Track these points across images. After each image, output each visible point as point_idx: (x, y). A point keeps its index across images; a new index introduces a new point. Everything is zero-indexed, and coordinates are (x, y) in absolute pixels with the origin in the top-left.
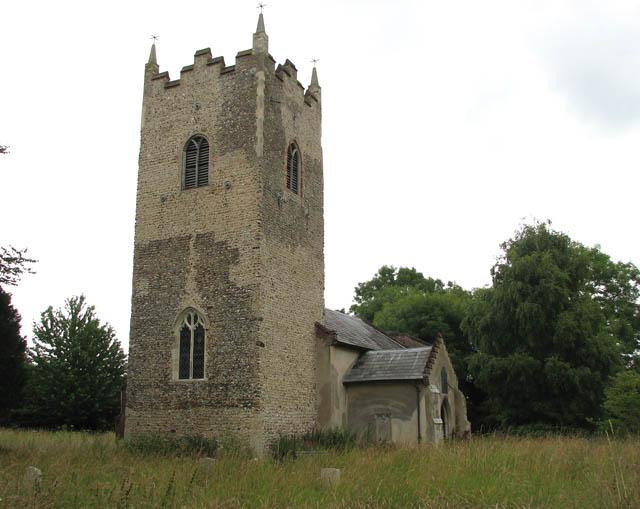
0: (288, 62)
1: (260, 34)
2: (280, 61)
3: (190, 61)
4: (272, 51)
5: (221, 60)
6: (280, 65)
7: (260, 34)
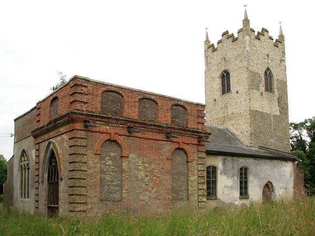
0: (263, 29)
1: (246, 21)
2: (258, 29)
3: (220, 38)
4: (252, 26)
5: (232, 35)
6: (276, 40)
7: (246, 21)
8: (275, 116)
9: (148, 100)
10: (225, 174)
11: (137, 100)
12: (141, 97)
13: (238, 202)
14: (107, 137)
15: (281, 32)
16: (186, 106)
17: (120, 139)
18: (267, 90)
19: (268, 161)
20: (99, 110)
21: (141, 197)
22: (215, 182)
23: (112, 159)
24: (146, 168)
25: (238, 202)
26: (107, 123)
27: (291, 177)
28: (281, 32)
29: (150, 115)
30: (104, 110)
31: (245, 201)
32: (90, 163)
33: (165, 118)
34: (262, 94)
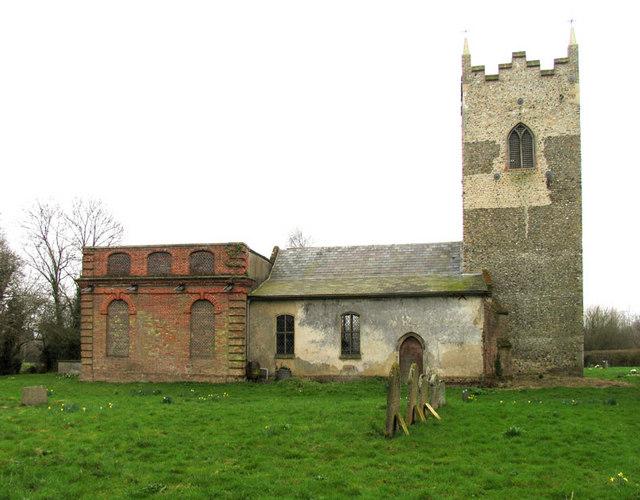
8: (533, 210)
9: (199, 252)
10: (310, 324)
11: (146, 255)
12: (150, 252)
13: (340, 365)
14: (111, 297)
15: (466, 46)
16: (213, 250)
17: (127, 298)
18: (514, 164)
19: (412, 303)
20: (105, 273)
21: (150, 354)
22: (291, 337)
23: (121, 317)
24: (156, 323)
25: (340, 365)
26: (110, 286)
27: (475, 323)
28: (466, 46)
29: (163, 268)
30: (192, 270)
31: (352, 363)
32: (97, 322)
33: (181, 268)
34: (497, 177)
